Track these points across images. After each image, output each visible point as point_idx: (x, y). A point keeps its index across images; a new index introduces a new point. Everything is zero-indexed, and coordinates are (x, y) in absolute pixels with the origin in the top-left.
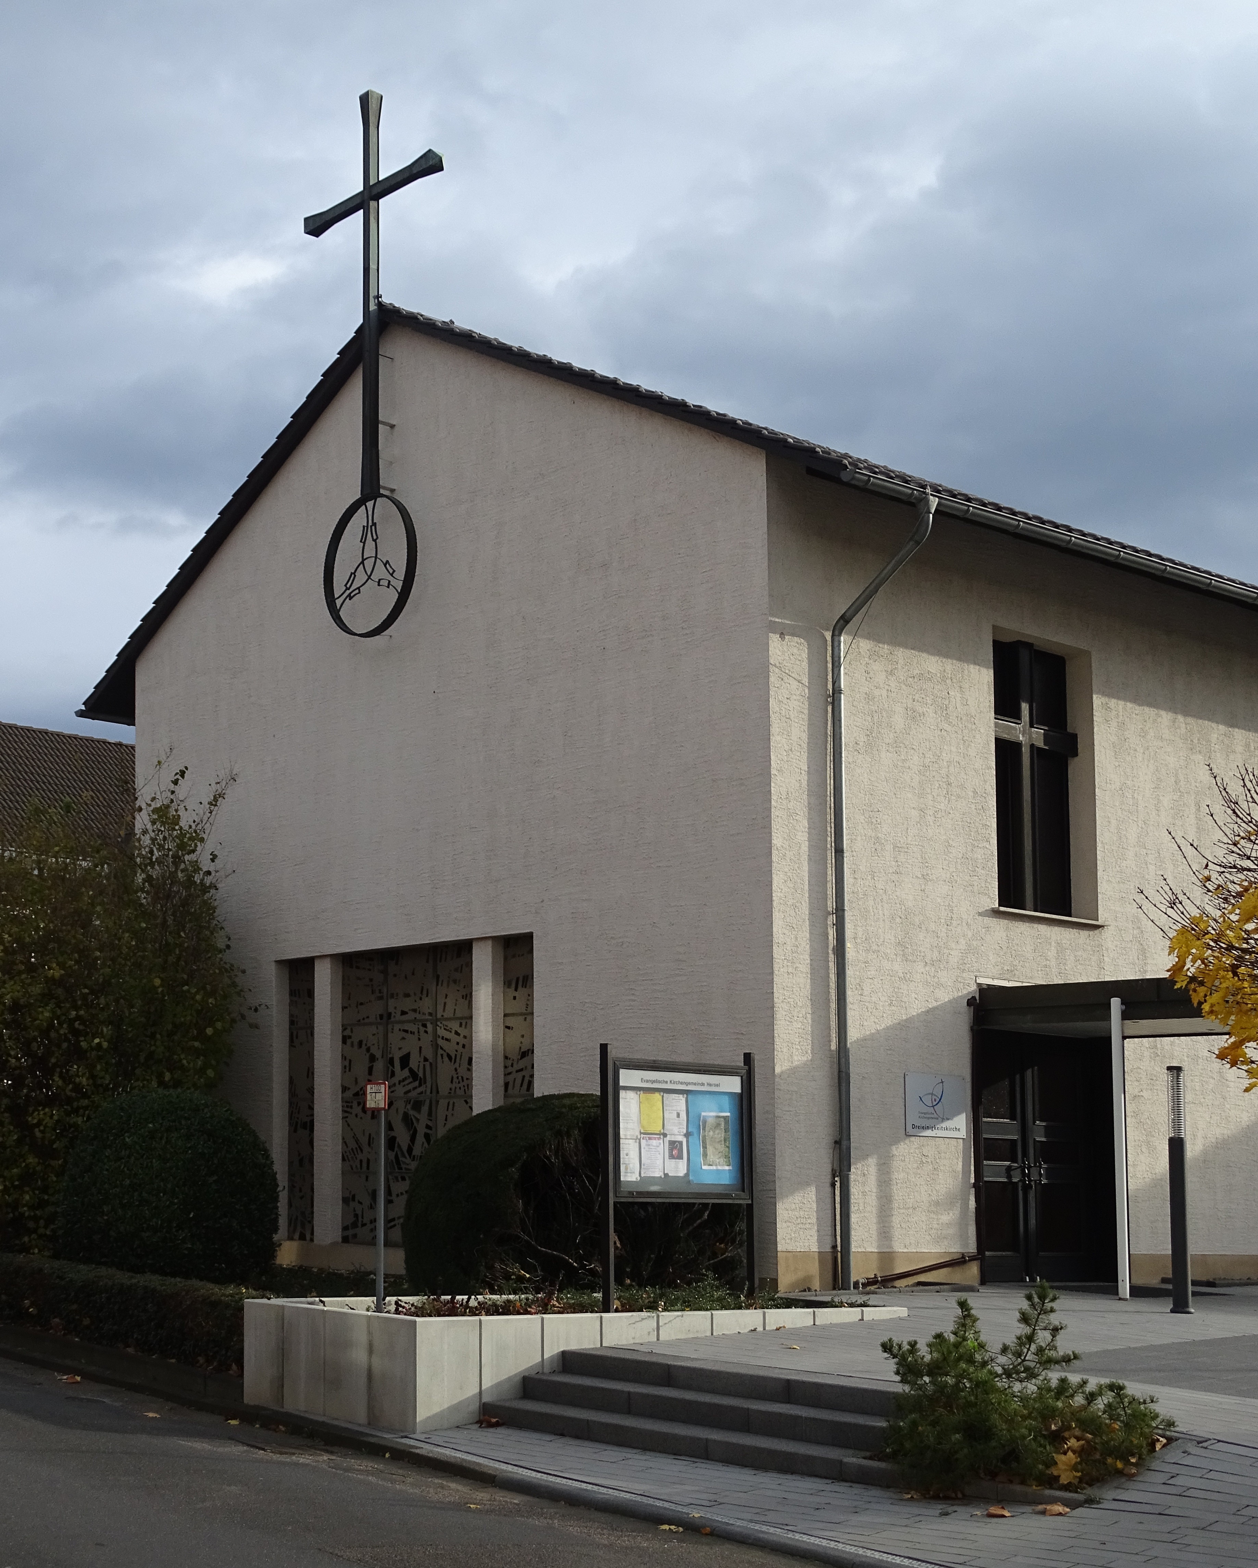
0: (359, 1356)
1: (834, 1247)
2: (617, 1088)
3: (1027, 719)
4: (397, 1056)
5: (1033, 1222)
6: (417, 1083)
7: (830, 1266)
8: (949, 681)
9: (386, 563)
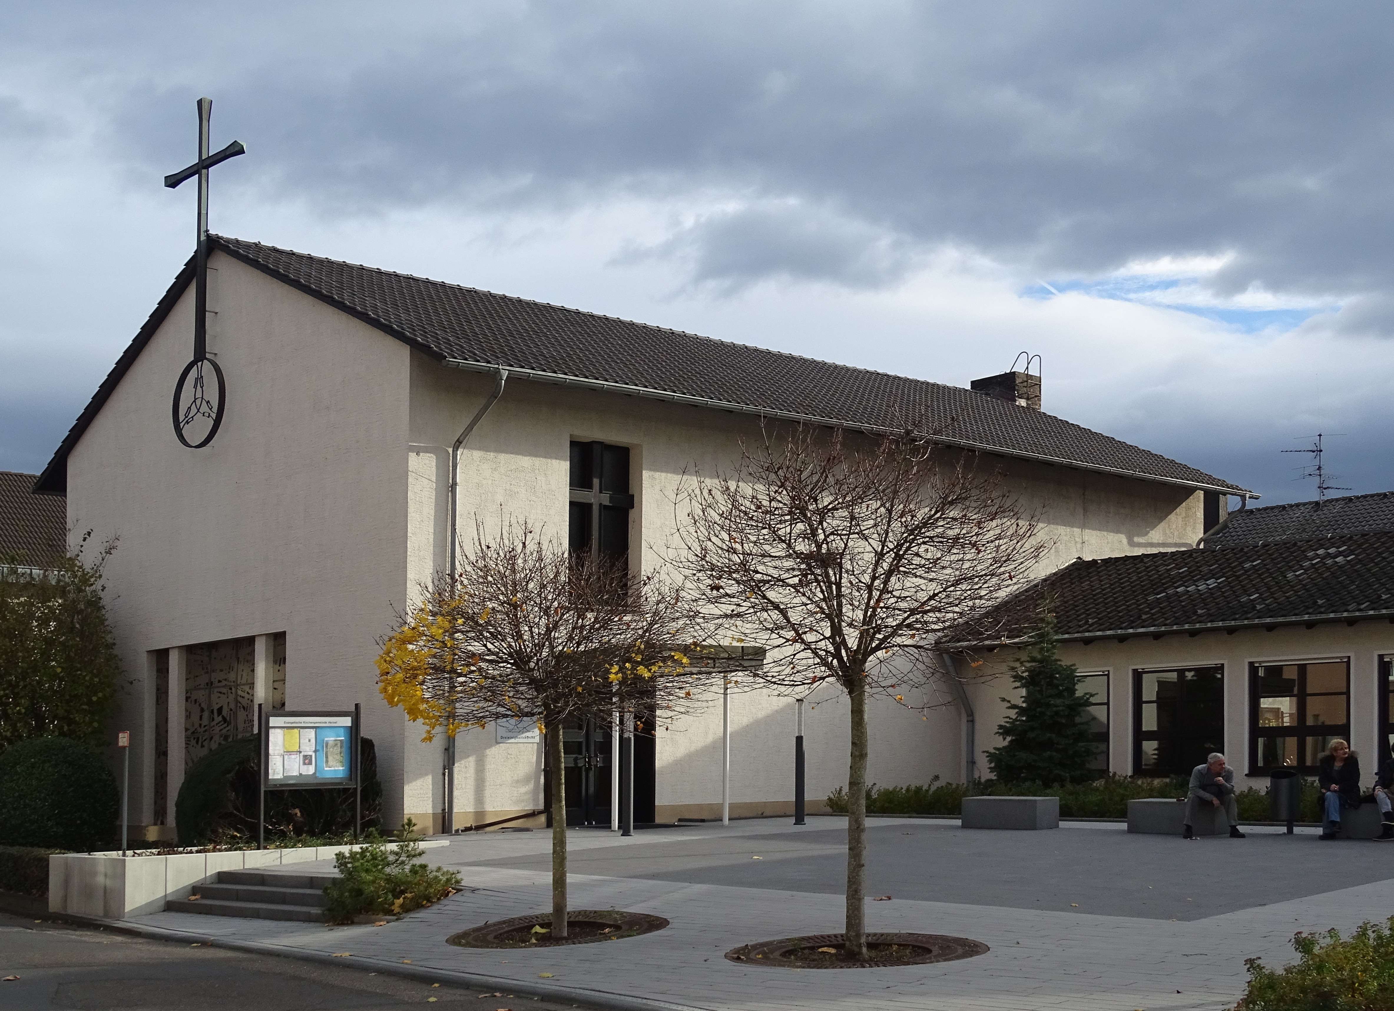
0: (100, 880)
1: (444, 810)
2: (268, 728)
3: (598, 489)
4: (216, 707)
5: (592, 789)
6: (226, 725)
7: (440, 821)
8: (537, 471)
9: (208, 402)
